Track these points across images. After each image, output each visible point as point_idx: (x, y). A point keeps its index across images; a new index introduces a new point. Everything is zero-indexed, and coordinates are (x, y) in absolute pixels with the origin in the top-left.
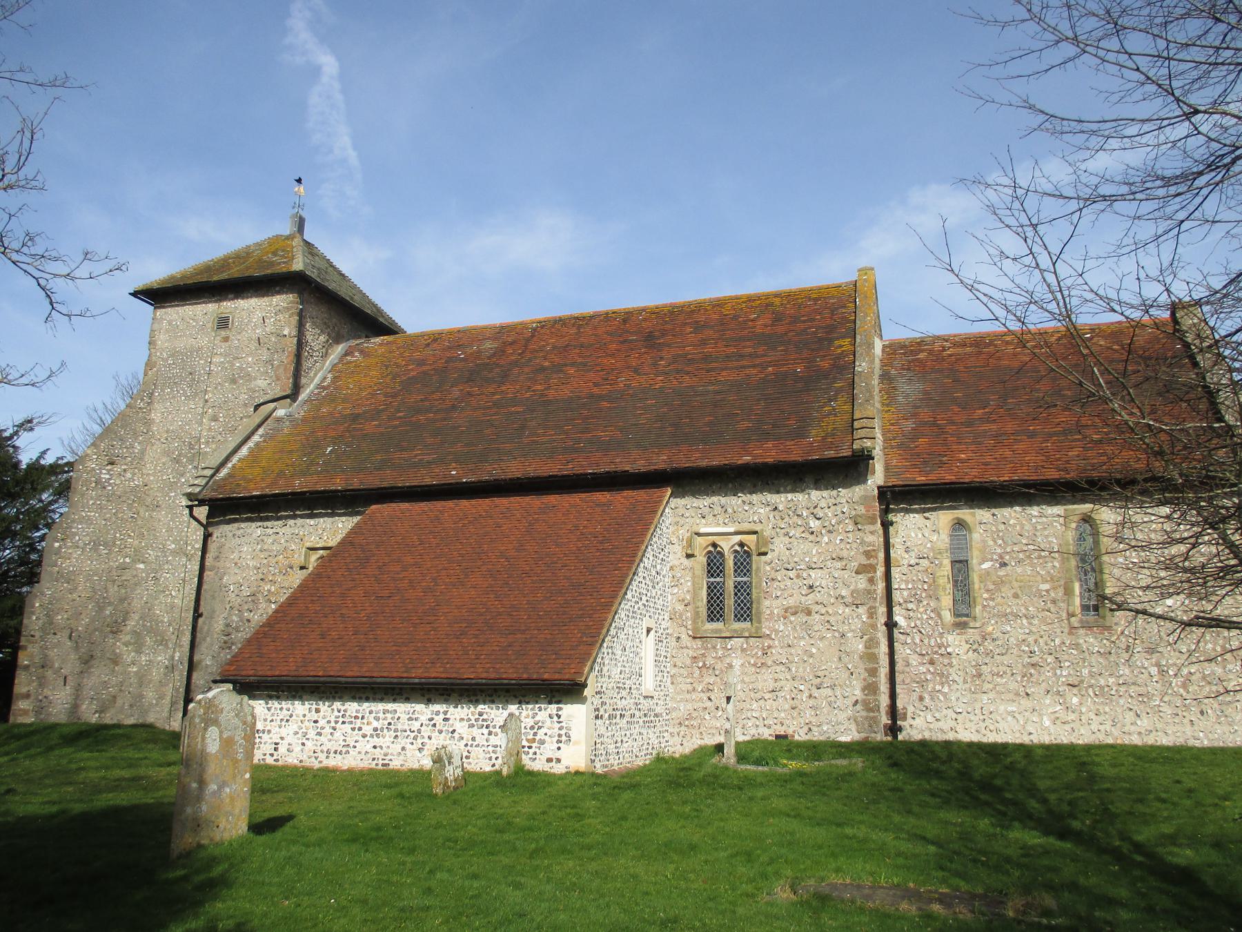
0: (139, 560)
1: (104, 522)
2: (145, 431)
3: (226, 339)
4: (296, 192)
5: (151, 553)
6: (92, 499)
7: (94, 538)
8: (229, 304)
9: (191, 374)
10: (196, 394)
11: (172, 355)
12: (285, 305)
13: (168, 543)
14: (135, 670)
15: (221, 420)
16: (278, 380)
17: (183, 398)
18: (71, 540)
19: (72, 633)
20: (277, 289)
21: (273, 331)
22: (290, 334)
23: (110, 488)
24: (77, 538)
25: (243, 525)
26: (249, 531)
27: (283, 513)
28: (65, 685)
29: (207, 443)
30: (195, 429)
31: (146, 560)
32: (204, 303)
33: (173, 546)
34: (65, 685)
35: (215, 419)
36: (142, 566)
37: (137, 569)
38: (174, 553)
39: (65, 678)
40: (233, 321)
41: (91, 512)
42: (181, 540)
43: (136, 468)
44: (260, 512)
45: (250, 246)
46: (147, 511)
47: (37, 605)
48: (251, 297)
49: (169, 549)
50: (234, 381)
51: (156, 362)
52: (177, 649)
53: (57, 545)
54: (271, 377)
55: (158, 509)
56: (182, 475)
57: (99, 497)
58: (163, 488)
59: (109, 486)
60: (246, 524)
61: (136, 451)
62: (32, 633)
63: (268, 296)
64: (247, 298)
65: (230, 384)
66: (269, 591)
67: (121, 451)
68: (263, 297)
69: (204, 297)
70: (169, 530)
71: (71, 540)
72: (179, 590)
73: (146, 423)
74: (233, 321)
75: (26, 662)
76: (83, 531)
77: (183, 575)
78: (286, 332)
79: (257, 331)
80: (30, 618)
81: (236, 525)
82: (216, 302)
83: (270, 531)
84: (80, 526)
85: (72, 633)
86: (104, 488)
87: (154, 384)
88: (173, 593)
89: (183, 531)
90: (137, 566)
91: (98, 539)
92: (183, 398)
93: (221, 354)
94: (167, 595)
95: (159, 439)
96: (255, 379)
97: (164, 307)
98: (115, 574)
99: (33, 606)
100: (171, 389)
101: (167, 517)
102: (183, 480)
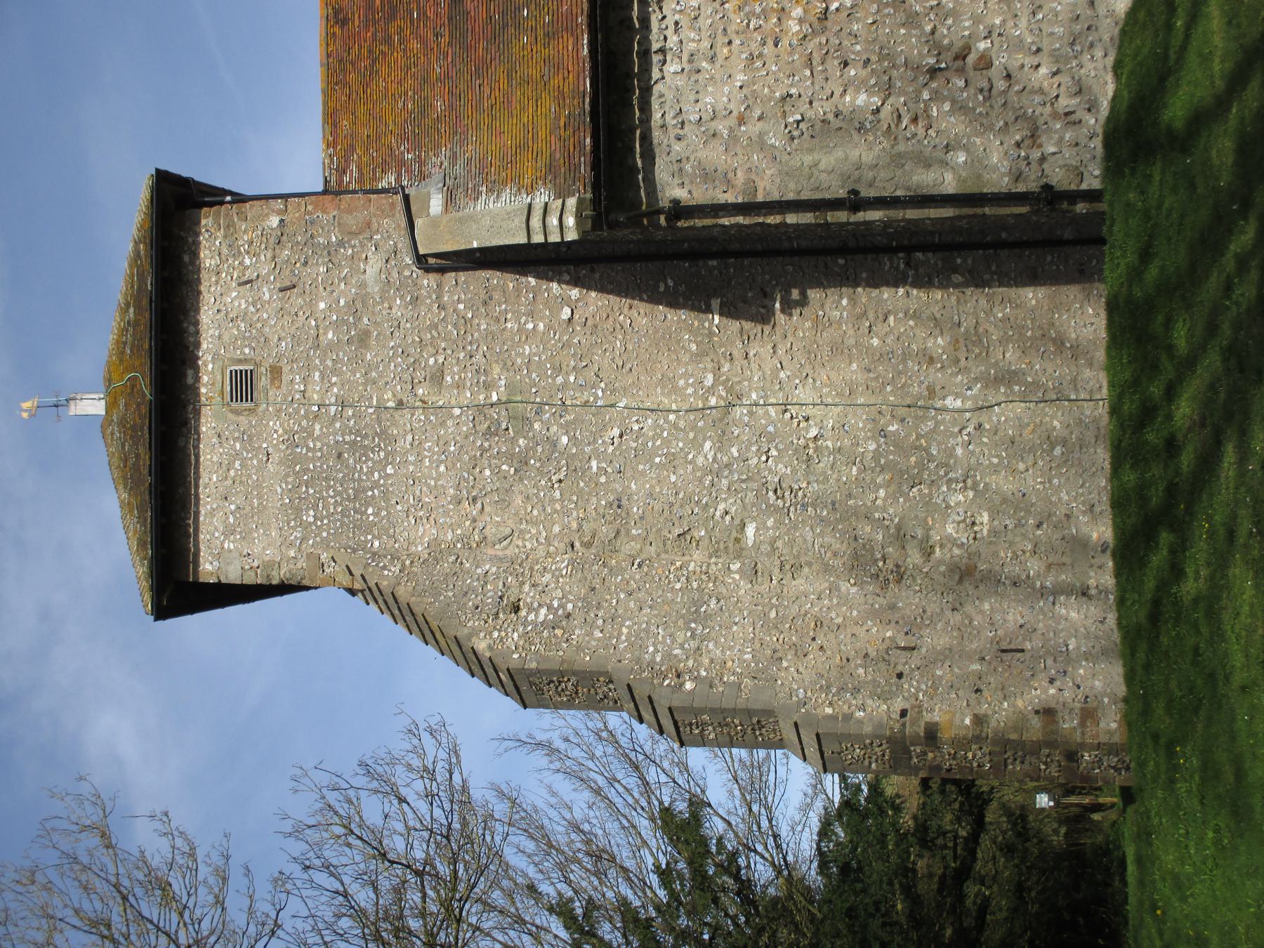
0: (737, 540)
1: (647, 611)
2: (453, 558)
3: (276, 372)
4: (31, 416)
5: (721, 507)
6: (590, 634)
7: (680, 623)
8: (205, 379)
9: (340, 456)
10: (383, 434)
11: (298, 511)
12: (220, 234)
13: (700, 461)
14: (985, 517)
15: (441, 360)
16: (369, 225)
17: (390, 470)
18: (680, 661)
19: (899, 648)
20: (186, 258)
21: (269, 255)
22: (279, 212)
23: (570, 606)
24: (677, 652)
25: (657, 116)
26: (669, 96)
27: (635, 13)
28: (1023, 651)
29: (488, 387)
30: (458, 425)
31: (737, 522)
32: (197, 447)
33: (708, 445)
34: (1023, 651)
35: (437, 378)
36: (750, 530)
37: (757, 546)
38: (722, 442)
39: (1004, 651)
40: (240, 361)
41: (620, 634)
42: (694, 427)
43: (532, 569)
44: (629, 75)
45: (122, 502)
46: (628, 532)
47: (829, 711)
48: (197, 323)
49: (715, 459)
50: (363, 339)
51: (309, 555)
52: (939, 404)
53: (689, 686)
54: (362, 245)
55: (625, 502)
56: (554, 444)
57: (589, 624)
58: (580, 494)
59: (565, 609)
60: (655, 105)
61: (494, 569)
62: (896, 716)
63: (199, 281)
64: (197, 332)
65: (367, 347)
66: (801, 21)
67: (490, 594)
68: (199, 293)
69: (186, 448)
70: (672, 462)
71: (680, 661)
72: (807, 419)
73: (436, 559)
74: (240, 361)
75: (967, 721)
76: (664, 642)
77: (772, 411)
78: (274, 221)
79: (267, 296)
80: (860, 722)
81: (656, 134)
82: (197, 413)
83: (673, 40)
84: (651, 649)
85: (899, 648)
86: (568, 616)
87: (354, 551)
88: (813, 432)
89: (675, 426)
90: (750, 543)
91: (683, 617)
92: (390, 470)
93: (305, 380)
94: (816, 449)
95: (474, 521)
96: (363, 285)
97: (197, 554)
98: (766, 585)
99: (833, 718)
100: (367, 505)
101: (643, 473)
102: (565, 440)
